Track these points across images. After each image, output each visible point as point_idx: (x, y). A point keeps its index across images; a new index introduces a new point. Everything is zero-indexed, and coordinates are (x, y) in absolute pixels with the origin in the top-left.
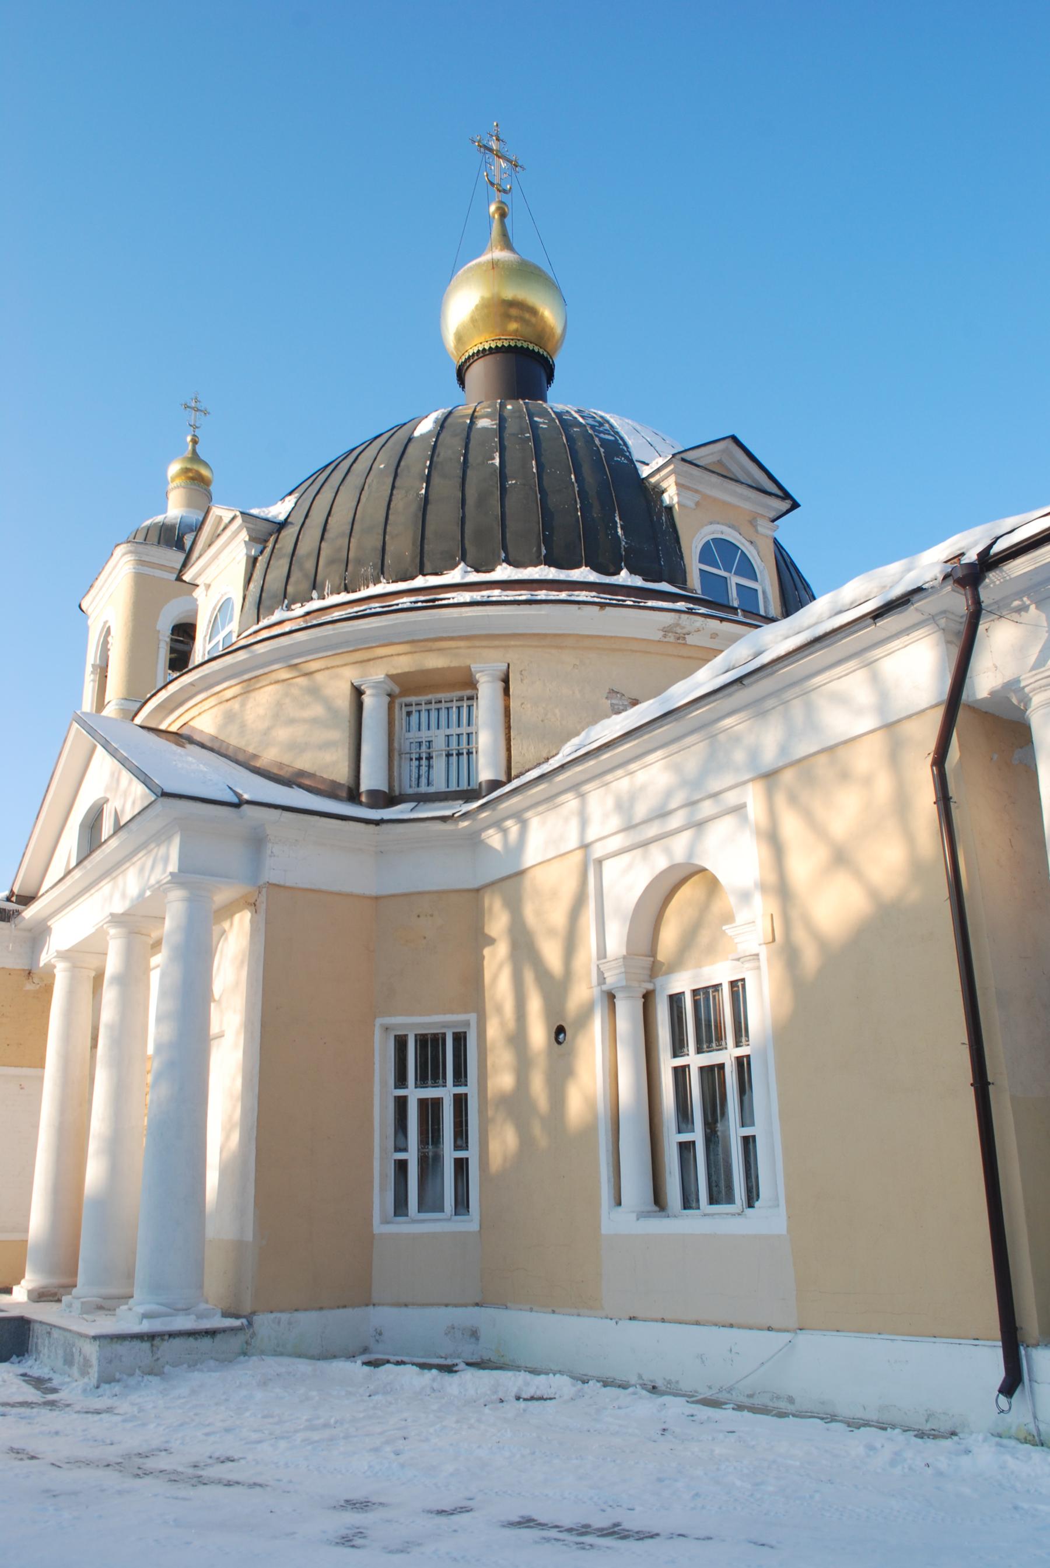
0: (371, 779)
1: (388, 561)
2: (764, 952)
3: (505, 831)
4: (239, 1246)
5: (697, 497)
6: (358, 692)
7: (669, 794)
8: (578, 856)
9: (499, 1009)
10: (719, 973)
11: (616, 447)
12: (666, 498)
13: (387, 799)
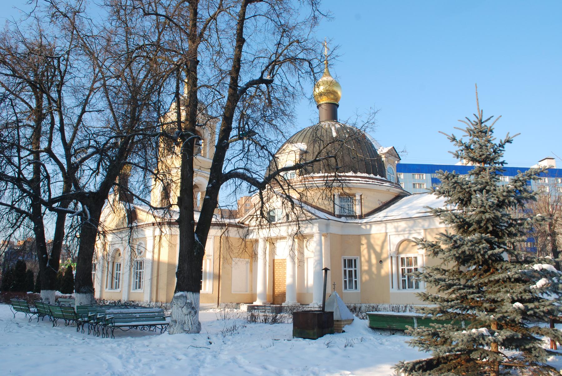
0: (337, 213)
7: (406, 228)
8: (384, 234)
9: (364, 256)
13: (340, 216)
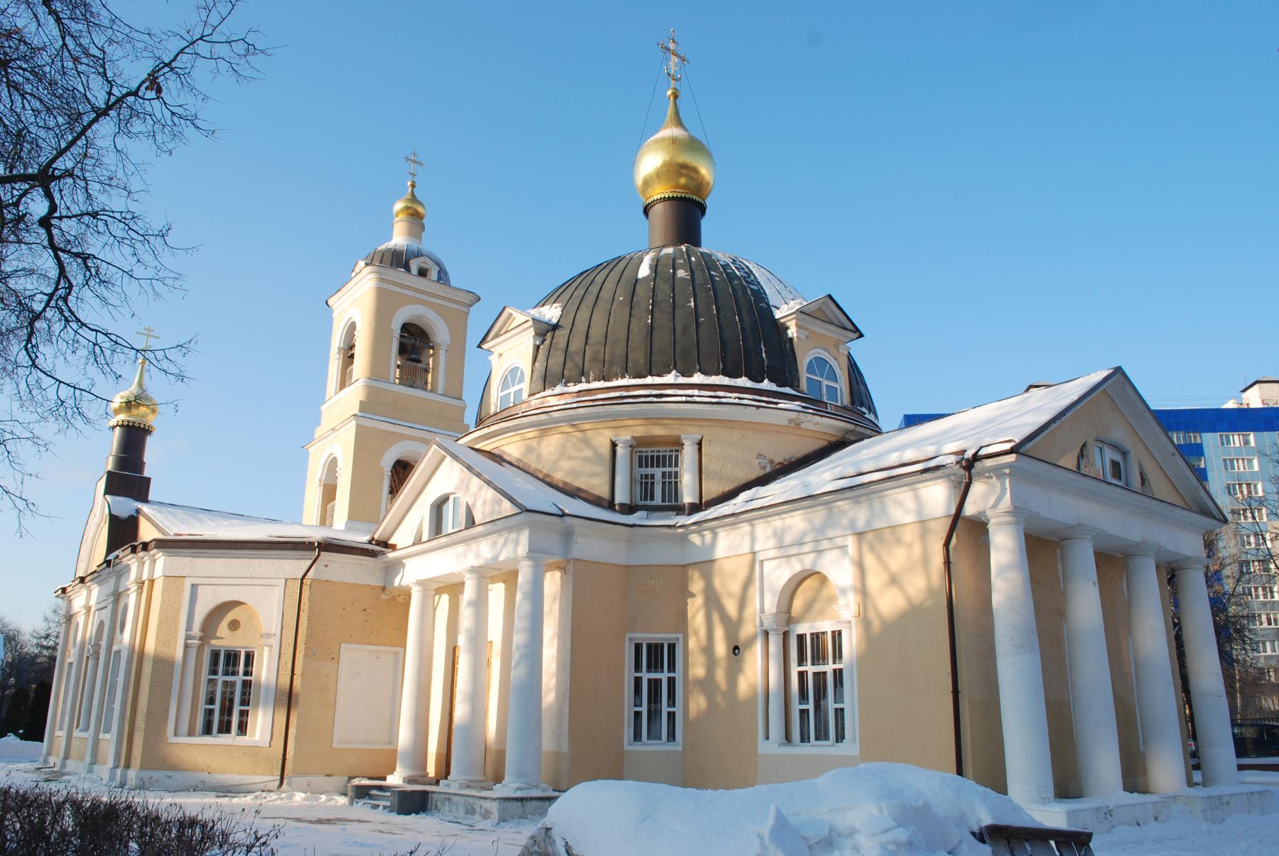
0: (621, 497)
1: (630, 365)
2: (853, 621)
3: (703, 537)
4: (557, 755)
5: (807, 333)
6: (614, 445)
7: (804, 533)
8: (749, 557)
9: (696, 633)
10: (826, 626)
11: (760, 296)
12: (789, 332)
13: (629, 509)
